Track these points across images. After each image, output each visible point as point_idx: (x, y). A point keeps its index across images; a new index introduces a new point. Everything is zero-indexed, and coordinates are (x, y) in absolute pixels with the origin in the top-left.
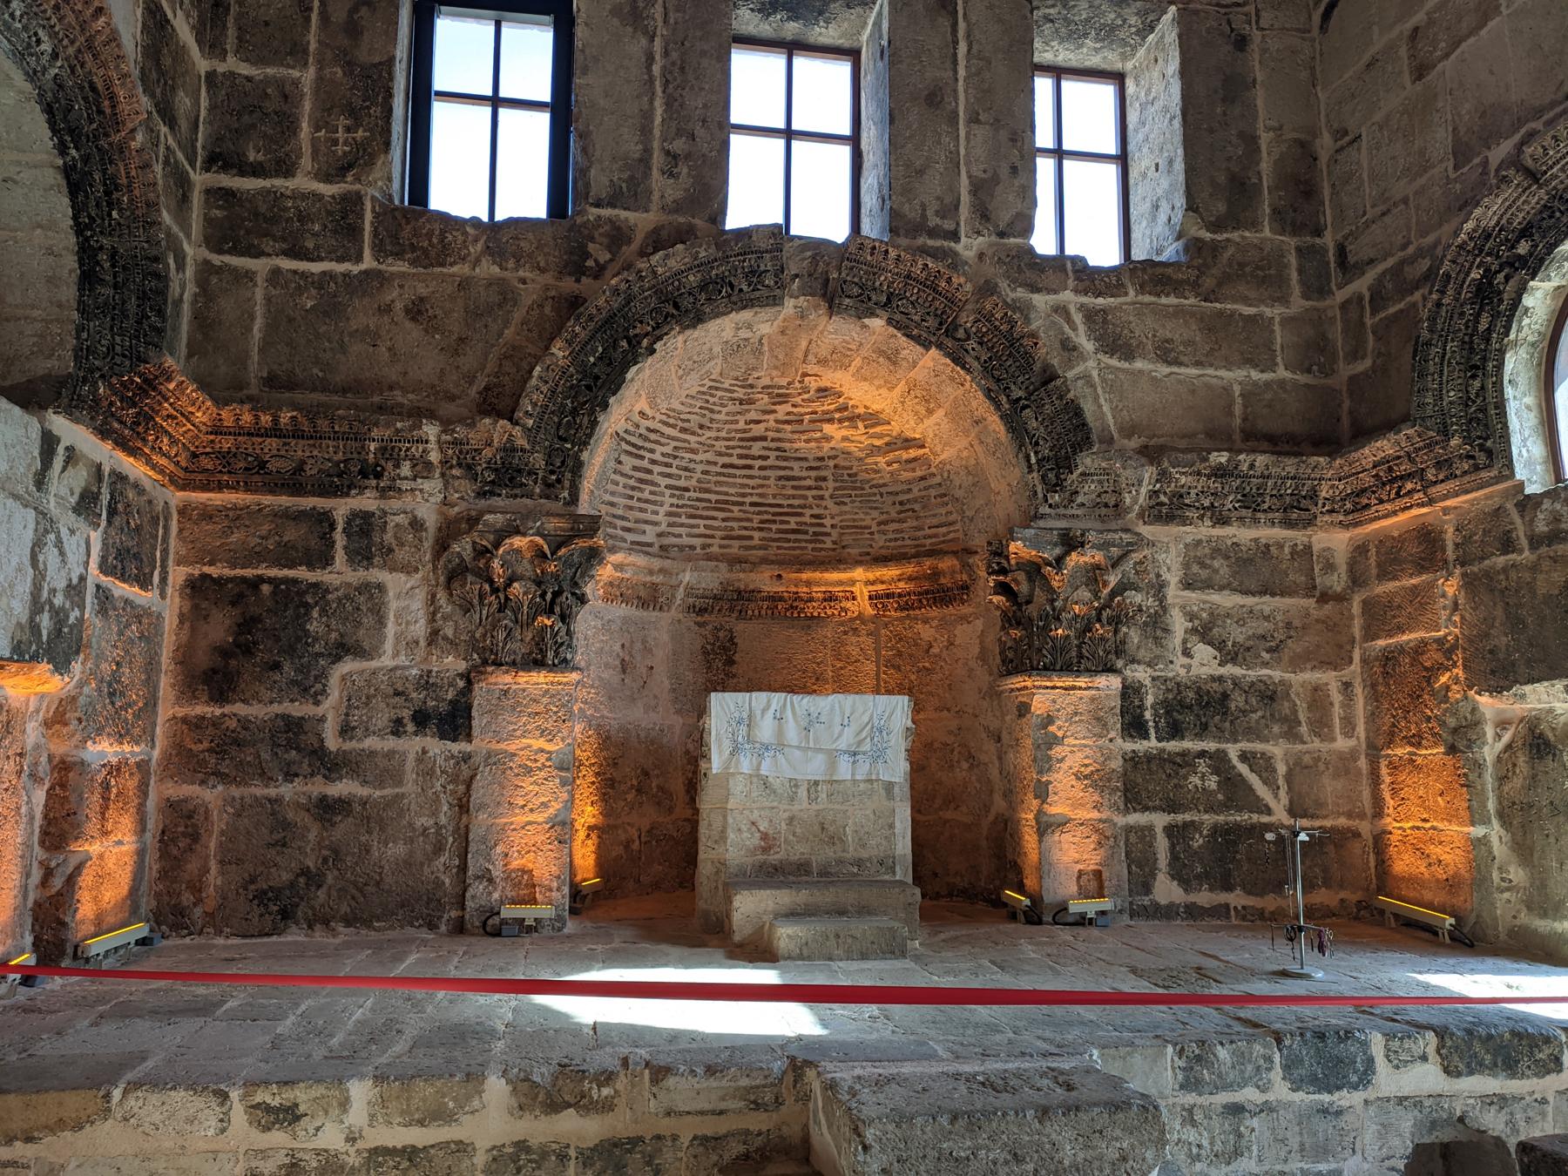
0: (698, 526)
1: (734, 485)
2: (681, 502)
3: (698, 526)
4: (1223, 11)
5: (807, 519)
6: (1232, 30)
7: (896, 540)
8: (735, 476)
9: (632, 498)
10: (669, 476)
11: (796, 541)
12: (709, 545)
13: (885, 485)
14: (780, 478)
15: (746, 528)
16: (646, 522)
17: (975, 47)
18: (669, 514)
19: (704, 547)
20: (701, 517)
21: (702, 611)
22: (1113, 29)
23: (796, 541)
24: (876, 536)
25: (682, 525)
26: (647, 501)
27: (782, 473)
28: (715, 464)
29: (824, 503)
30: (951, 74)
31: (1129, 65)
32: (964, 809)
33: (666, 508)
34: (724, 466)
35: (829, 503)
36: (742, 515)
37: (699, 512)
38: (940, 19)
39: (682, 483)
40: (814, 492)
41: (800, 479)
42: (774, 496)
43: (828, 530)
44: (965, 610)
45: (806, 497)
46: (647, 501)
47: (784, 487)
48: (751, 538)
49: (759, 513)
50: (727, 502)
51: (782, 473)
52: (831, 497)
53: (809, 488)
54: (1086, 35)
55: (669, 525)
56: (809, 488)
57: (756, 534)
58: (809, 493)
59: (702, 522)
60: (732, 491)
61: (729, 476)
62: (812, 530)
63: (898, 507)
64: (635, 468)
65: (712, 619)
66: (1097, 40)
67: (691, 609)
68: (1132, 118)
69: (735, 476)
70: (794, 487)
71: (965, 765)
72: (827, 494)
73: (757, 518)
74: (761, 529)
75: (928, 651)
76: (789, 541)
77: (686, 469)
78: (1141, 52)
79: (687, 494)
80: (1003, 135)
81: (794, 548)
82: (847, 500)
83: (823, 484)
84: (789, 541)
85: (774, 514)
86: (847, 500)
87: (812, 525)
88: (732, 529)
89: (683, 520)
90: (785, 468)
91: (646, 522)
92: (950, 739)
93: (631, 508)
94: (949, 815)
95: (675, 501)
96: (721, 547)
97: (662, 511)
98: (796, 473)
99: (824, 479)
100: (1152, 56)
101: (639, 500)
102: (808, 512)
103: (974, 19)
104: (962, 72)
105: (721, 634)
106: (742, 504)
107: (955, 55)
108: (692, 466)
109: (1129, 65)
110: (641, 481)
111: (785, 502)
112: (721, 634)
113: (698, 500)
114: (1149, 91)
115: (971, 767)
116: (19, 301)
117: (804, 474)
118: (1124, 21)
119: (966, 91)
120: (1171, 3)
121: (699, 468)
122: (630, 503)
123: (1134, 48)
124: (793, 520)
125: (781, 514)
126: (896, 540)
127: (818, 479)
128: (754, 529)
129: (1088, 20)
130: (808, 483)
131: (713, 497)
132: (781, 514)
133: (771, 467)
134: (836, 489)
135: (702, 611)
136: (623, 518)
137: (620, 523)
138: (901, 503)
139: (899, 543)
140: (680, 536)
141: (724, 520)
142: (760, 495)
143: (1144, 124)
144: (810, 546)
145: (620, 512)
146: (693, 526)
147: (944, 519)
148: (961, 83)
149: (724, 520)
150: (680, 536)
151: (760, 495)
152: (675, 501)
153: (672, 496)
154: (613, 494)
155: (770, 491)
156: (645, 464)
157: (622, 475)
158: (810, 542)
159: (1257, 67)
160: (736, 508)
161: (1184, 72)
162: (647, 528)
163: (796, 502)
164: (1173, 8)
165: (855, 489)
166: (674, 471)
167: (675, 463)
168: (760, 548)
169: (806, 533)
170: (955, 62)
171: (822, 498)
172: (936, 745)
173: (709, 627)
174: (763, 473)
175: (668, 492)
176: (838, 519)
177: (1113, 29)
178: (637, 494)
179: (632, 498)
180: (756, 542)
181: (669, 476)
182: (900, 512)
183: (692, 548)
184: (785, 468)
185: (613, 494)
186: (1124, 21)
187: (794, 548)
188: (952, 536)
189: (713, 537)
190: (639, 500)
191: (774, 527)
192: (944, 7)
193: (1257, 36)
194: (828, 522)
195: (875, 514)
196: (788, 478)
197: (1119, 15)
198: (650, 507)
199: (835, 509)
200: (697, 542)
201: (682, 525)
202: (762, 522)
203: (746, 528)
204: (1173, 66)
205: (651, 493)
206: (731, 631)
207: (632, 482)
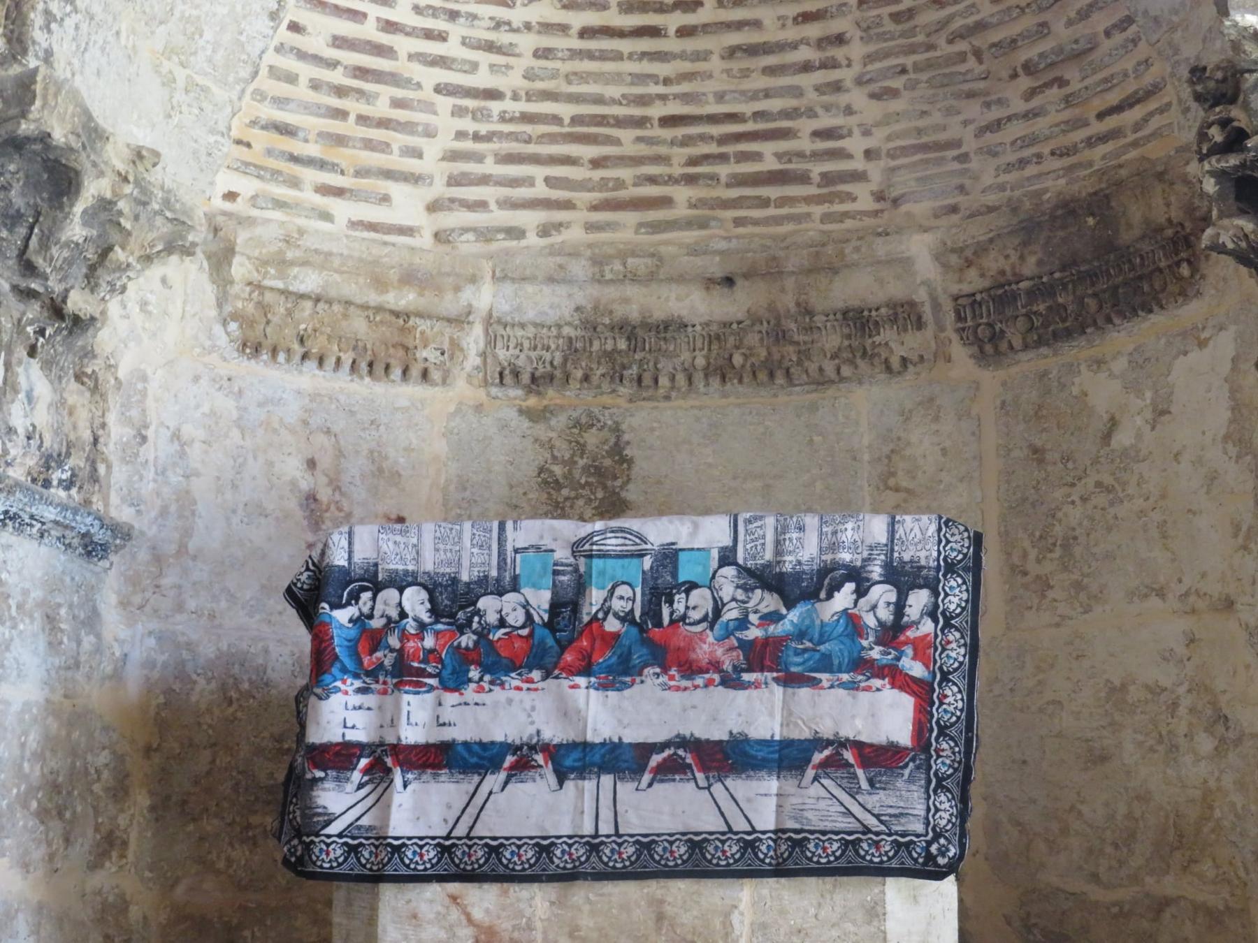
0: (529, 182)
1: (617, 78)
2: (483, 129)
3: (529, 182)
5: (805, 144)
7: (1023, 163)
8: (618, 56)
9: (341, 114)
10: (441, 62)
11: (783, 201)
12: (559, 226)
13: (981, 26)
14: (731, 53)
15: (652, 180)
16: (389, 174)
18: (453, 156)
19: (544, 231)
20: (536, 160)
21: (537, 382)
23: (783, 201)
24: (974, 164)
25: (484, 180)
26: (384, 123)
27: (735, 38)
28: (563, 29)
29: (843, 99)
32: (1206, 867)
33: (447, 141)
34: (585, 33)
35: (857, 97)
36: (643, 149)
37: (532, 149)
39: (483, 80)
40: (819, 77)
41: (781, 47)
42: (720, 97)
43: (858, 164)
44: (1191, 312)
45: (797, 92)
46: (384, 123)
47: (745, 74)
48: (666, 202)
49: (686, 141)
50: (601, 120)
51: (735, 38)
52: (860, 82)
53: (806, 67)
55: (454, 181)
56: (806, 67)
57: (682, 194)
58: (807, 81)
59: (539, 172)
60: (613, 91)
61: (603, 56)
62: (817, 169)
63: (1025, 82)
64: (339, 42)
65: (571, 400)
67: (507, 375)
69: (618, 56)
70: (770, 71)
71: (1206, 744)
72: (846, 75)
73: (680, 154)
74: (691, 180)
75: (1107, 437)
76: (765, 203)
77: (490, 47)
79: (496, 107)
81: (778, 220)
82: (897, 83)
83: (838, 53)
84: (765, 203)
85: (724, 140)
86: (897, 83)
87: (816, 156)
88: (620, 184)
89: (490, 167)
90: (739, 25)
91: (389, 174)
92: (1165, 676)
93: (340, 140)
94: (1169, 885)
95: (468, 125)
96: (590, 227)
97: (432, 150)
98: (772, 34)
99: (840, 39)
101: (362, 119)
102: (806, 126)
105: (592, 439)
106: (641, 122)
108: (504, 38)
110: (362, 72)
111: (747, 108)
112: (592, 439)
113: (527, 118)
115: (1221, 749)
117: (791, 34)
121: (526, 43)
122: (336, 126)
124: (768, 148)
125: (739, 137)
126: (1023, 163)
127: (822, 43)
128: (672, 180)
130: (805, 54)
131: (566, 110)
132: (739, 137)
133: (706, 28)
134: (869, 58)
135: (537, 382)
136: (322, 165)
137: (311, 176)
138: (1029, 68)
139: (1031, 170)
140: (481, 205)
141: (596, 163)
142: (686, 98)
144: (818, 210)
145: (313, 150)
146: (514, 182)
147: (1131, 87)
149: (596, 163)
150: (481, 205)
151: (686, 98)
152: (468, 125)
153: (458, 112)
154: (280, 102)
155: (710, 87)
156: (369, 31)
157: (302, 55)
158: (819, 200)
160: (626, 135)
162: (396, 190)
163: (775, 105)
165: (912, 50)
166: (453, 48)
167: (456, 31)
168: (689, 224)
169: (804, 179)
171: (837, 87)
172: (1134, 694)
173: (560, 421)
174: (690, 45)
175: (445, 103)
176: (879, 136)
178: (353, 106)
179: (341, 114)
180: (680, 211)
181: (441, 62)
182: (1031, 94)
183: (515, 233)
184: (739, 25)
185: (280, 102)
187: (778, 220)
188: (1155, 123)
189: (568, 205)
190: (362, 119)
191: (723, 171)
194: (855, 144)
195: (973, 110)
196: (753, 50)
198: (398, 139)
199: (871, 111)
200: (530, 219)
201: (484, 180)
202: (693, 162)
203: (652, 180)
205: (397, 104)
206: (617, 430)
207: (337, 77)
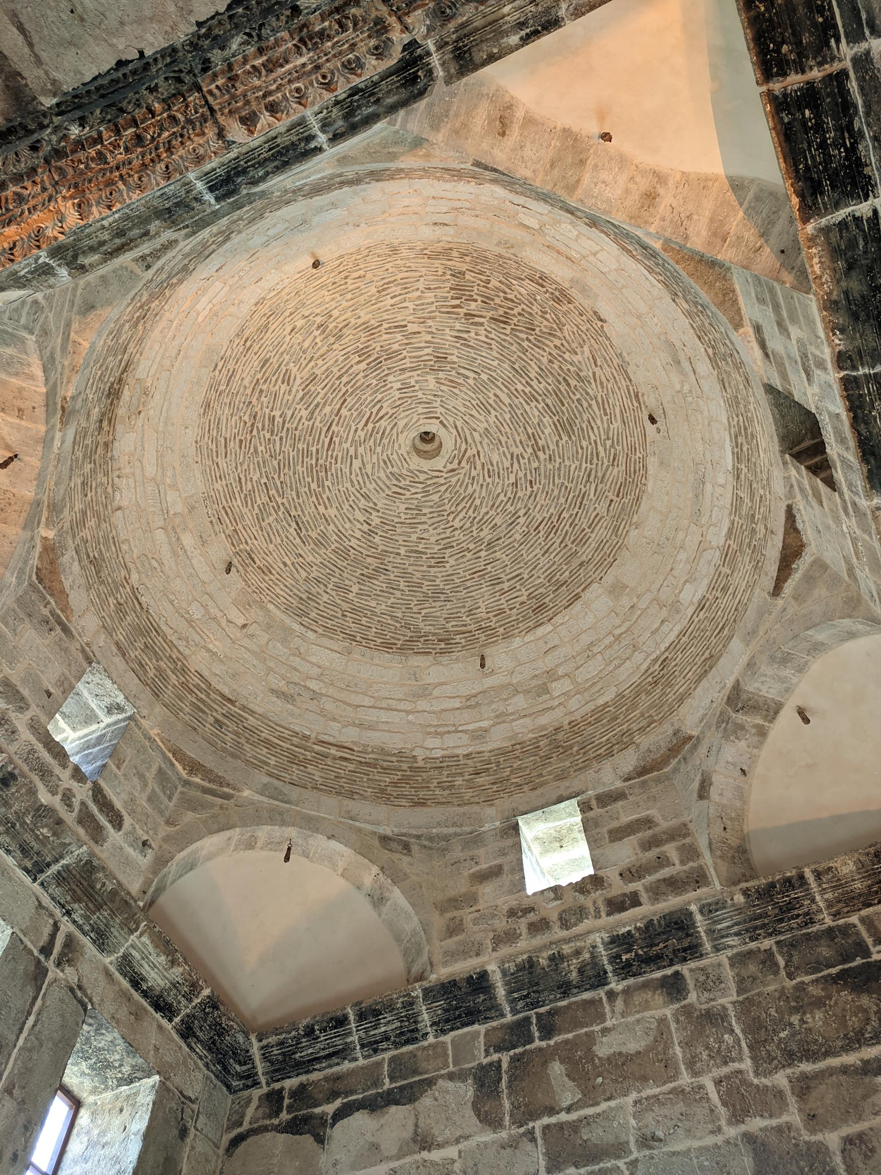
4: (183, 1099)
6: (182, 1119)
17: (39, 1027)
22: (109, 1066)
30: (14, 1037)
31: (91, 1099)
38: (29, 987)
54: (87, 1059)
66: (91, 1067)
68: (75, 1147)
78: (109, 1095)
80: (22, 1119)
100: (119, 1105)
103: (48, 1003)
104: (21, 1042)
107: (25, 1023)
109: (91, 1099)
114: (103, 1133)
116: (97, 217)
118: (121, 1065)
119: (16, 1060)
120: (158, 1073)
123: (106, 1089)
129: (100, 1049)
143: (86, 1160)
148: (16, 1051)
159: (185, 1159)
161: (148, 1136)
164: (157, 1078)
170: (21, 1030)
177: (109, 1066)
186: (121, 1065)
192: (36, 979)
193: (192, 1131)
197: (121, 1060)
204: (140, 1124)
